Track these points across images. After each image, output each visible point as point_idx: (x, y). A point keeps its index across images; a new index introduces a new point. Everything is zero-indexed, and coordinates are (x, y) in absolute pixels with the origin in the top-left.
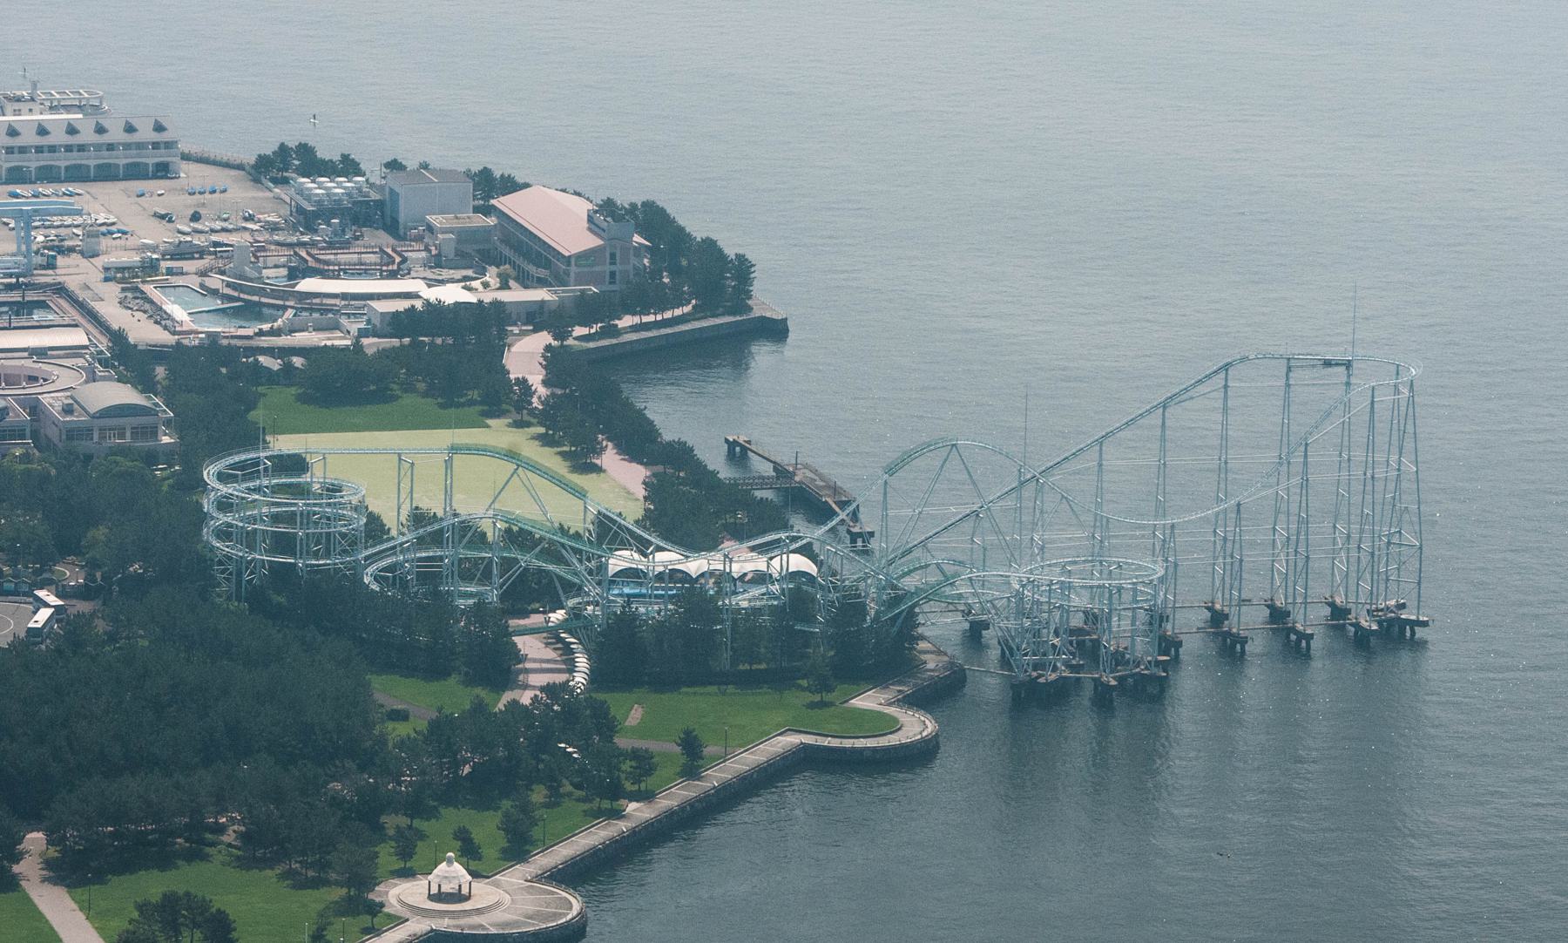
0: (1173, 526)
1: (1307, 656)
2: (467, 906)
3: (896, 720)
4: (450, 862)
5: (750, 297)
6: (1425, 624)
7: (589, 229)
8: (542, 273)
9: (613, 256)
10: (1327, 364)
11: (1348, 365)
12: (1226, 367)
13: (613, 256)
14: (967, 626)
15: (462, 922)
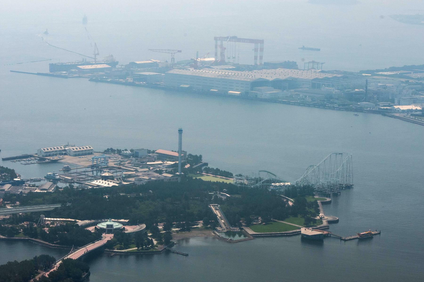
11: (342, 154)
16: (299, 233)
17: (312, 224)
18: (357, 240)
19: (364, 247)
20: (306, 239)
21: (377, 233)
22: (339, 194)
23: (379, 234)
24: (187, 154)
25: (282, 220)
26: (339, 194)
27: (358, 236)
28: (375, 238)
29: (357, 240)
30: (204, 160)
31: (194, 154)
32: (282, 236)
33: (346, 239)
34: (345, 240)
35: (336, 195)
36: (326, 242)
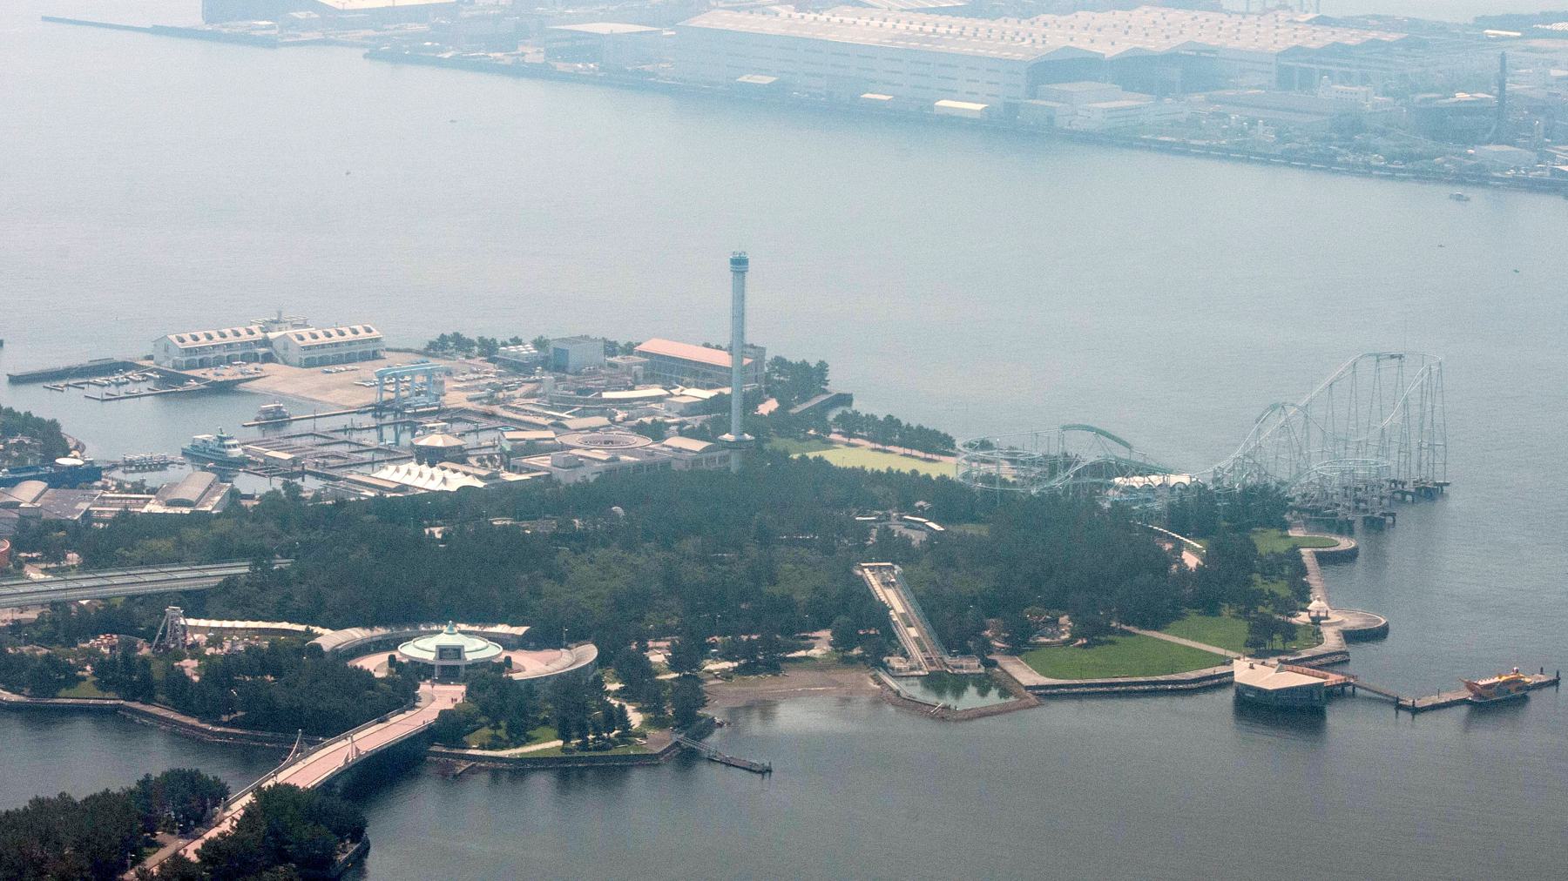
10: (1392, 357)
11: (1400, 357)
17: (1279, 645)
21: (1544, 679)
24: (769, 357)
25: (1156, 628)
26: (1389, 520)
27: (1466, 694)
29: (1464, 710)
31: (795, 359)
34: (1415, 711)
35: (1376, 525)
36: (1337, 718)
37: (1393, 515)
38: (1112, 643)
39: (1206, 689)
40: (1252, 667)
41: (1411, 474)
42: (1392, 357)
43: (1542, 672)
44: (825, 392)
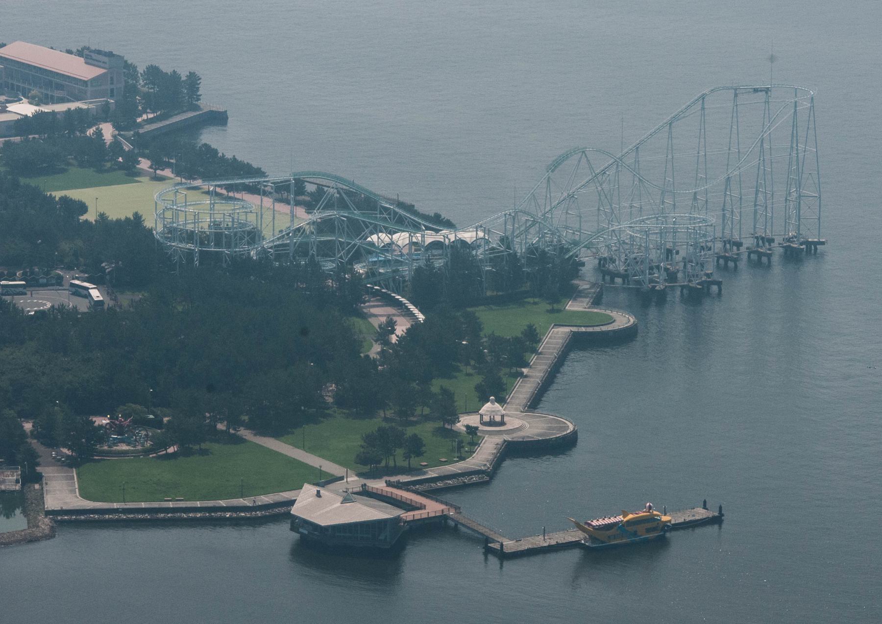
0: (695, 193)
1: (769, 266)
2: (502, 428)
3: (611, 318)
4: (492, 403)
5: (199, 100)
6: (823, 243)
7: (86, 63)
8: (57, 94)
9: (112, 79)
10: (756, 90)
11: (767, 90)
12: (703, 97)
13: (112, 79)
14: (597, 261)
15: (514, 435)
16: (281, 513)
17: (402, 463)
18: (575, 555)
19: (602, 593)
20: (323, 549)
21: (701, 513)
22: (715, 288)
23: (717, 520)
24: (141, 70)
25: (277, 433)
26: (715, 288)
27: (574, 536)
28: (678, 541)
29: (575, 555)
30: (208, 101)
31: (166, 69)
32: (212, 520)
33: (510, 545)
34: (504, 556)
35: (697, 296)
36: (421, 567)
37: (719, 284)
38: (204, 452)
39: (236, 523)
40: (318, 495)
41: (780, 232)
42: (756, 90)
43: (705, 507)
44: (197, 108)
